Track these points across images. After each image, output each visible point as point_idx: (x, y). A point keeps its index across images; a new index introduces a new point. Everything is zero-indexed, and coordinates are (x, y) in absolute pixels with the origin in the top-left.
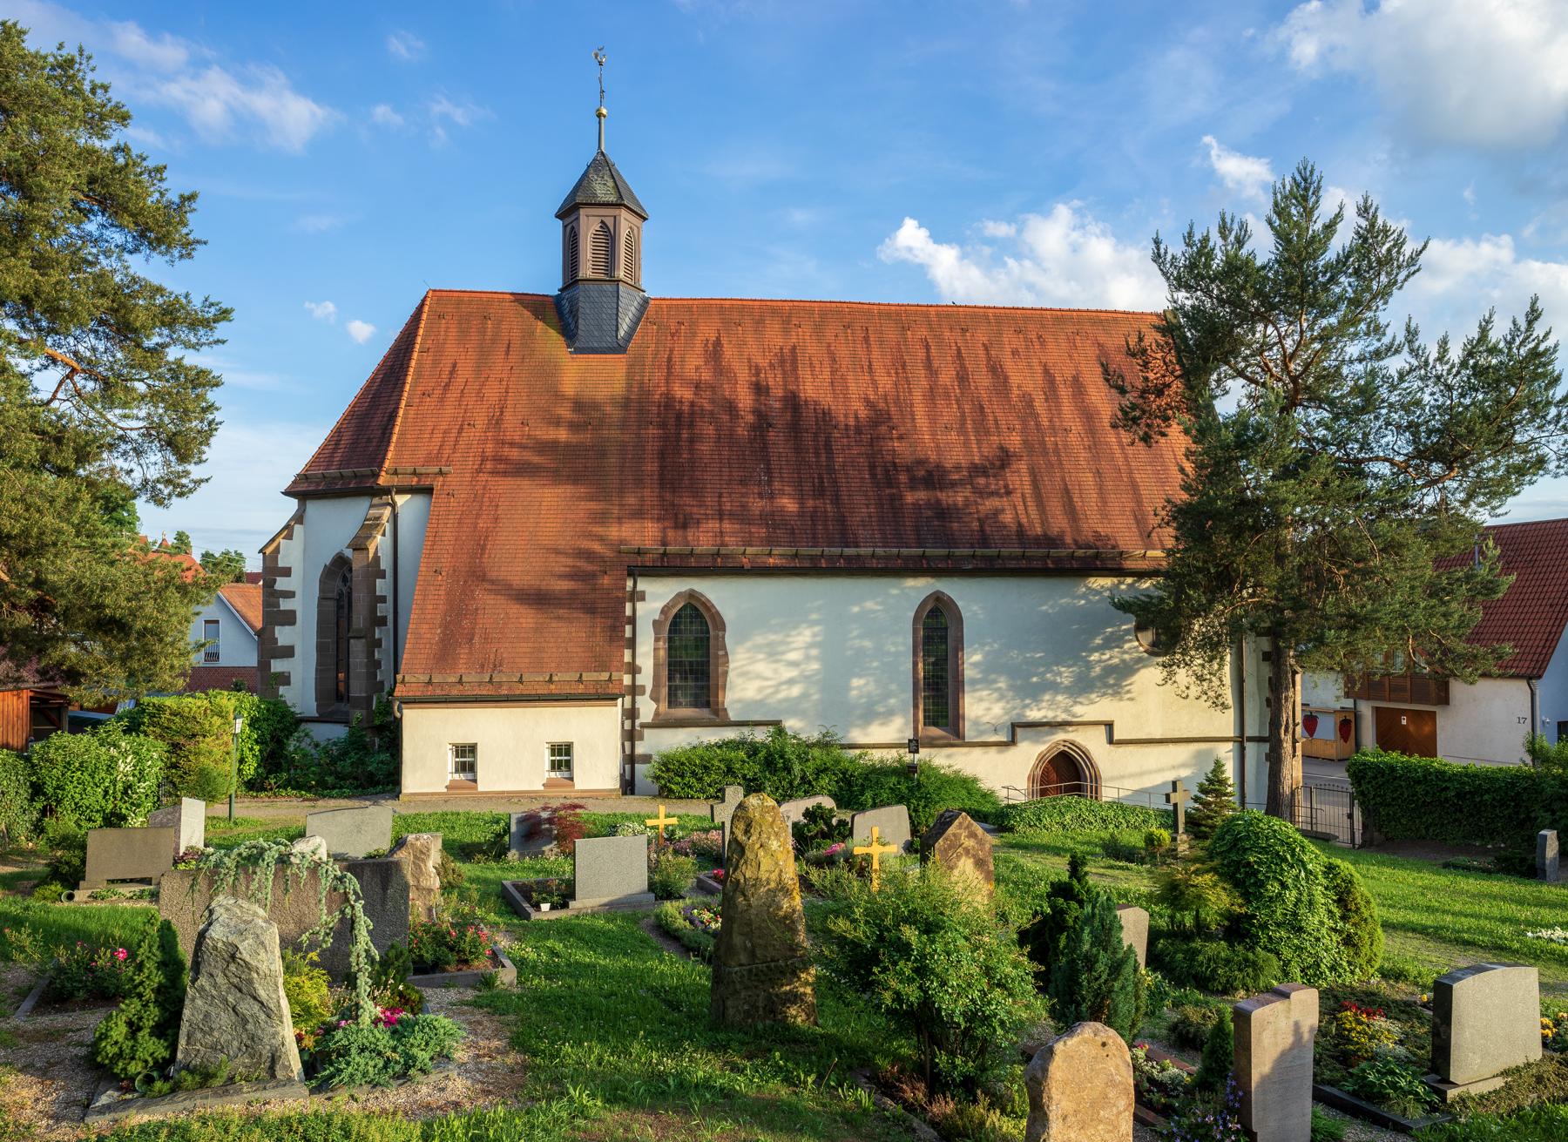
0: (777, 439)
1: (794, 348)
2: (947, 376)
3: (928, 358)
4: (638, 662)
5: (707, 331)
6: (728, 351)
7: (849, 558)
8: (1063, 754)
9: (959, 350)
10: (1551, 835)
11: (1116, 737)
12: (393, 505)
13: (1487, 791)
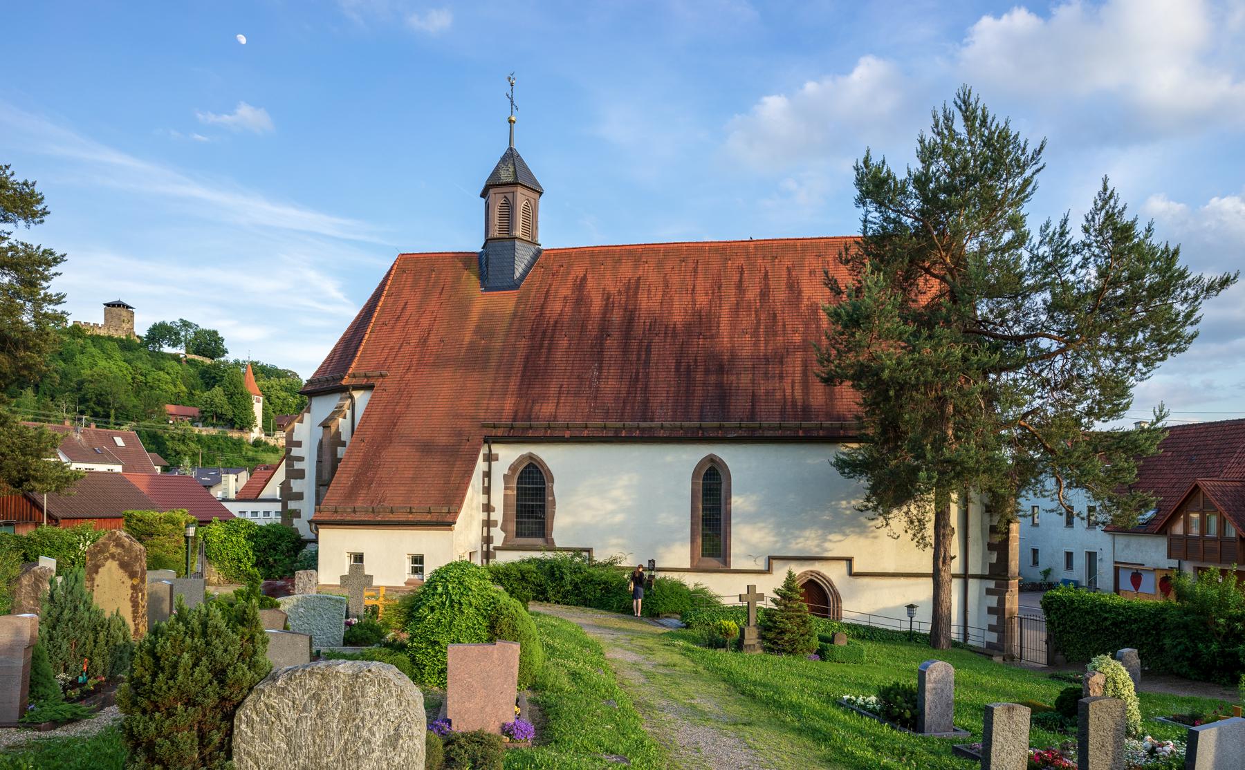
0: (612, 343)
1: (639, 278)
2: (752, 294)
3: (741, 281)
4: (492, 504)
5: (578, 271)
6: (590, 284)
7: (643, 430)
8: (811, 581)
9: (766, 273)
12: (352, 397)
13: (1135, 621)
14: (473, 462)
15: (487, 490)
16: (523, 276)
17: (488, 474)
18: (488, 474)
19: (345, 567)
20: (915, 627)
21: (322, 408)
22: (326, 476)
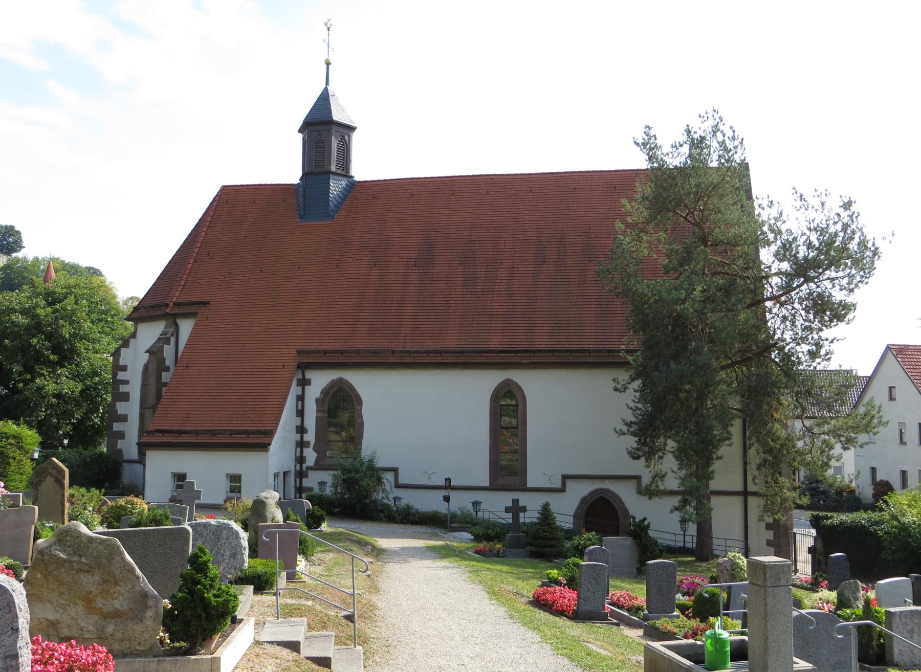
10: (54, 459)
11: (559, 485)
15: (301, 413)
17: (301, 398)
20: (687, 545)
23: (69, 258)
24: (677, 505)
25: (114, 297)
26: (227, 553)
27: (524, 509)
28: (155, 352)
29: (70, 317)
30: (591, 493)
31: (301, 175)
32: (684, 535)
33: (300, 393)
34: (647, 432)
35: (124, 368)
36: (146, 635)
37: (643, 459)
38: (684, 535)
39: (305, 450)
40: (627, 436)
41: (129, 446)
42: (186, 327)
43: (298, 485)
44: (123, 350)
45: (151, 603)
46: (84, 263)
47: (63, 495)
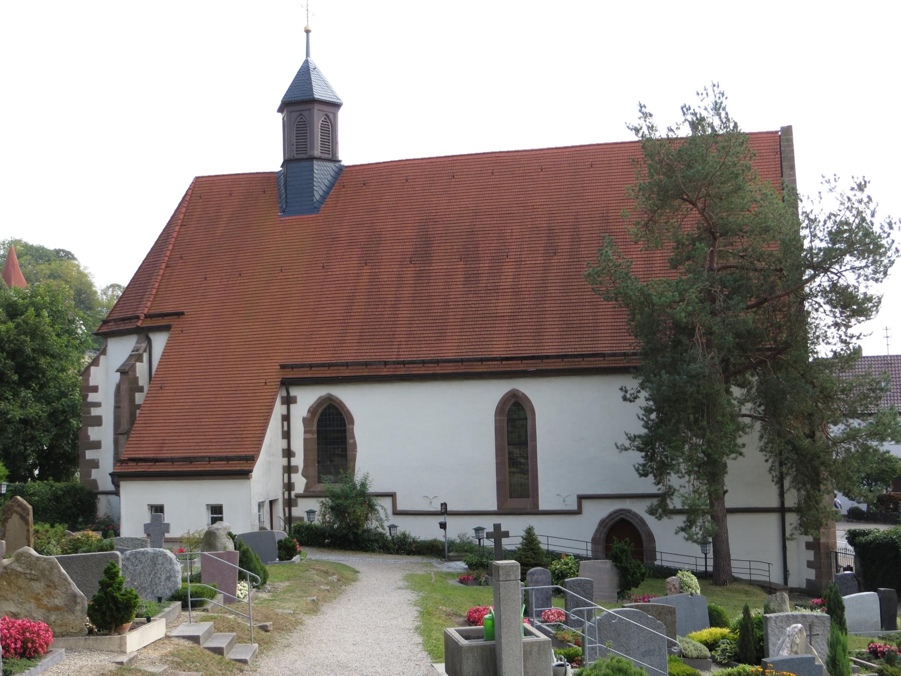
10: (19, 497)
11: (575, 507)
14: (271, 408)
15: (287, 435)
16: (324, 198)
17: (286, 418)
18: (286, 418)
19: (146, 517)
21: (120, 350)
22: (125, 425)
23: (34, 240)
24: (683, 525)
25: (91, 285)
26: (163, 577)
27: (506, 535)
28: (126, 371)
29: (34, 332)
30: (610, 515)
31: (282, 161)
32: (706, 558)
33: (285, 413)
34: (656, 447)
35: (95, 389)
36: (77, 622)
37: (651, 476)
38: (706, 558)
39: (293, 475)
40: (630, 451)
41: (102, 477)
42: (159, 342)
43: (287, 515)
44: (92, 368)
45: (79, 600)
46: (51, 245)
47: (28, 531)
